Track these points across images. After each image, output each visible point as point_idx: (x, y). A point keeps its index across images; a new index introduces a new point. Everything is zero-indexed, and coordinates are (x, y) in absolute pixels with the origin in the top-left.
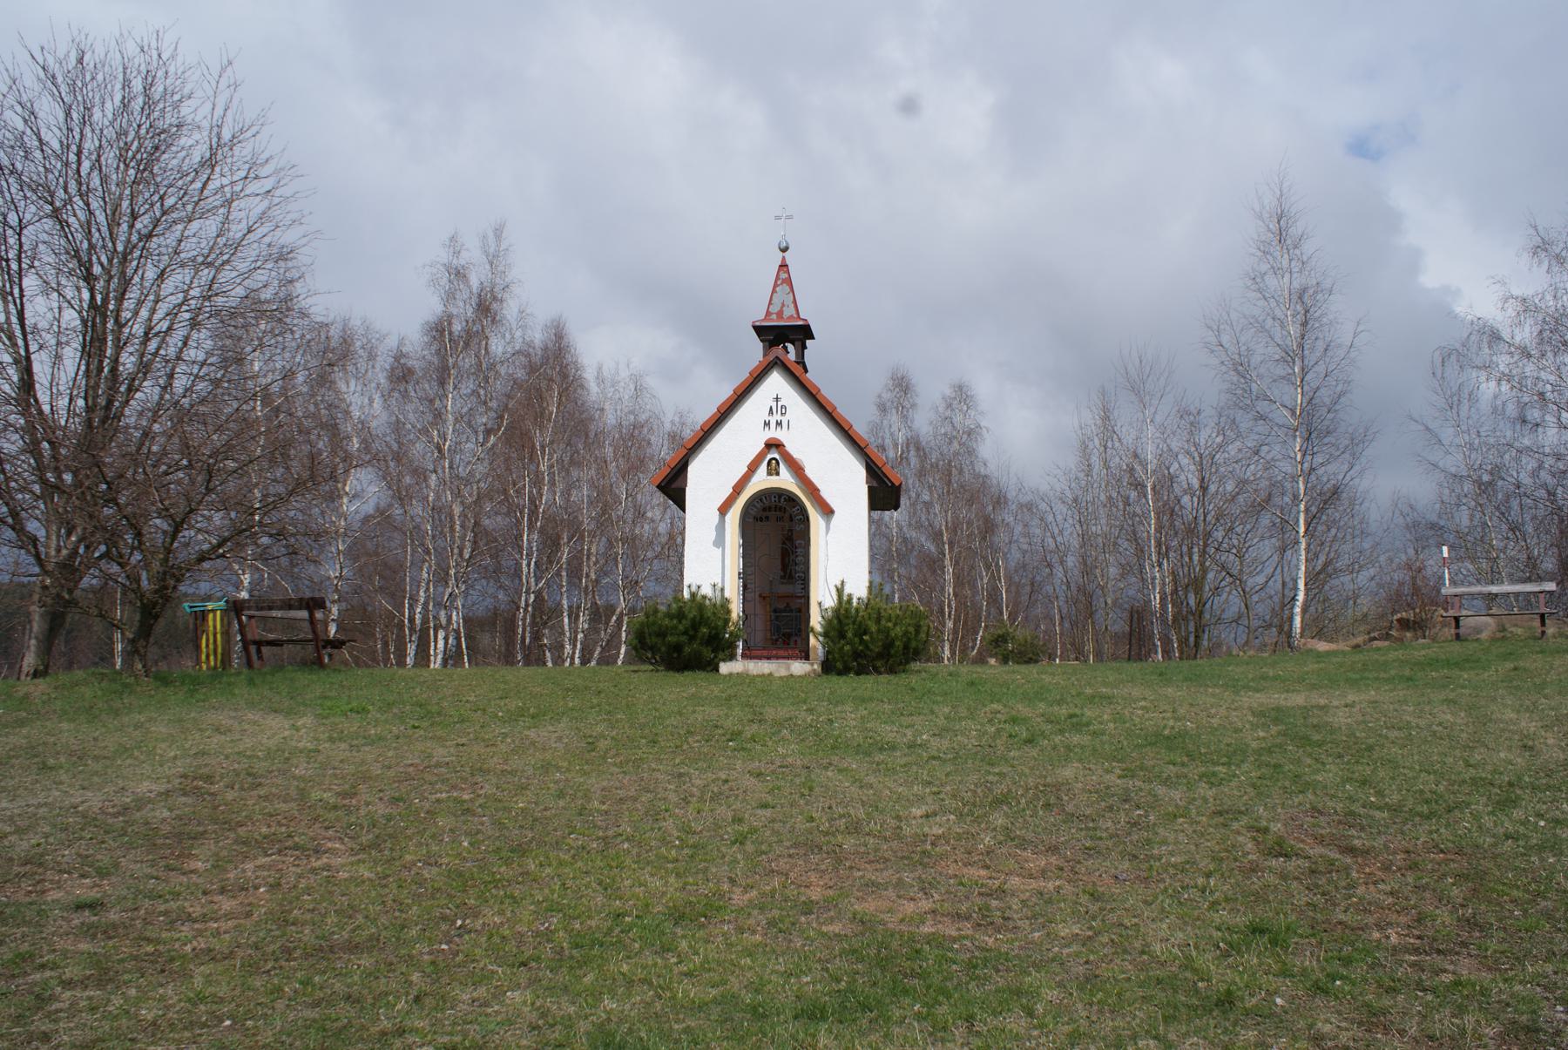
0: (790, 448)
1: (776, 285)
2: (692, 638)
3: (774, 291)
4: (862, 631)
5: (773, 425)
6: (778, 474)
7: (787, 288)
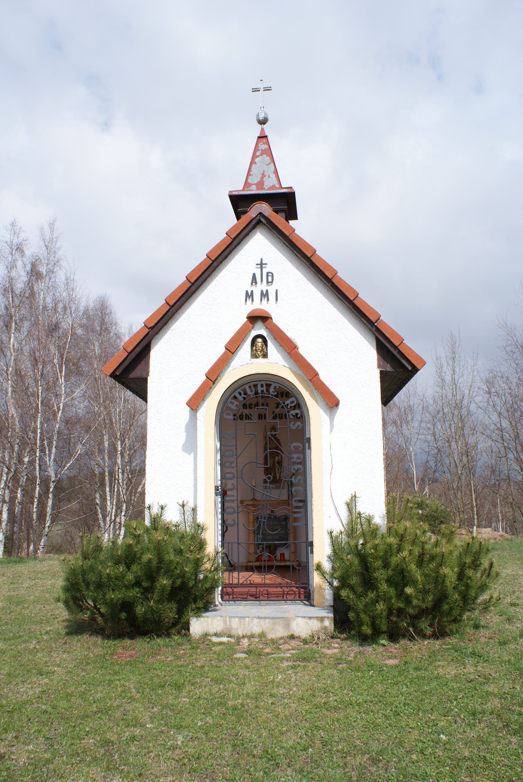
0: (276, 320)
1: (254, 156)
2: (147, 591)
3: (252, 162)
4: (400, 579)
5: (257, 296)
6: (265, 356)
7: (268, 159)
